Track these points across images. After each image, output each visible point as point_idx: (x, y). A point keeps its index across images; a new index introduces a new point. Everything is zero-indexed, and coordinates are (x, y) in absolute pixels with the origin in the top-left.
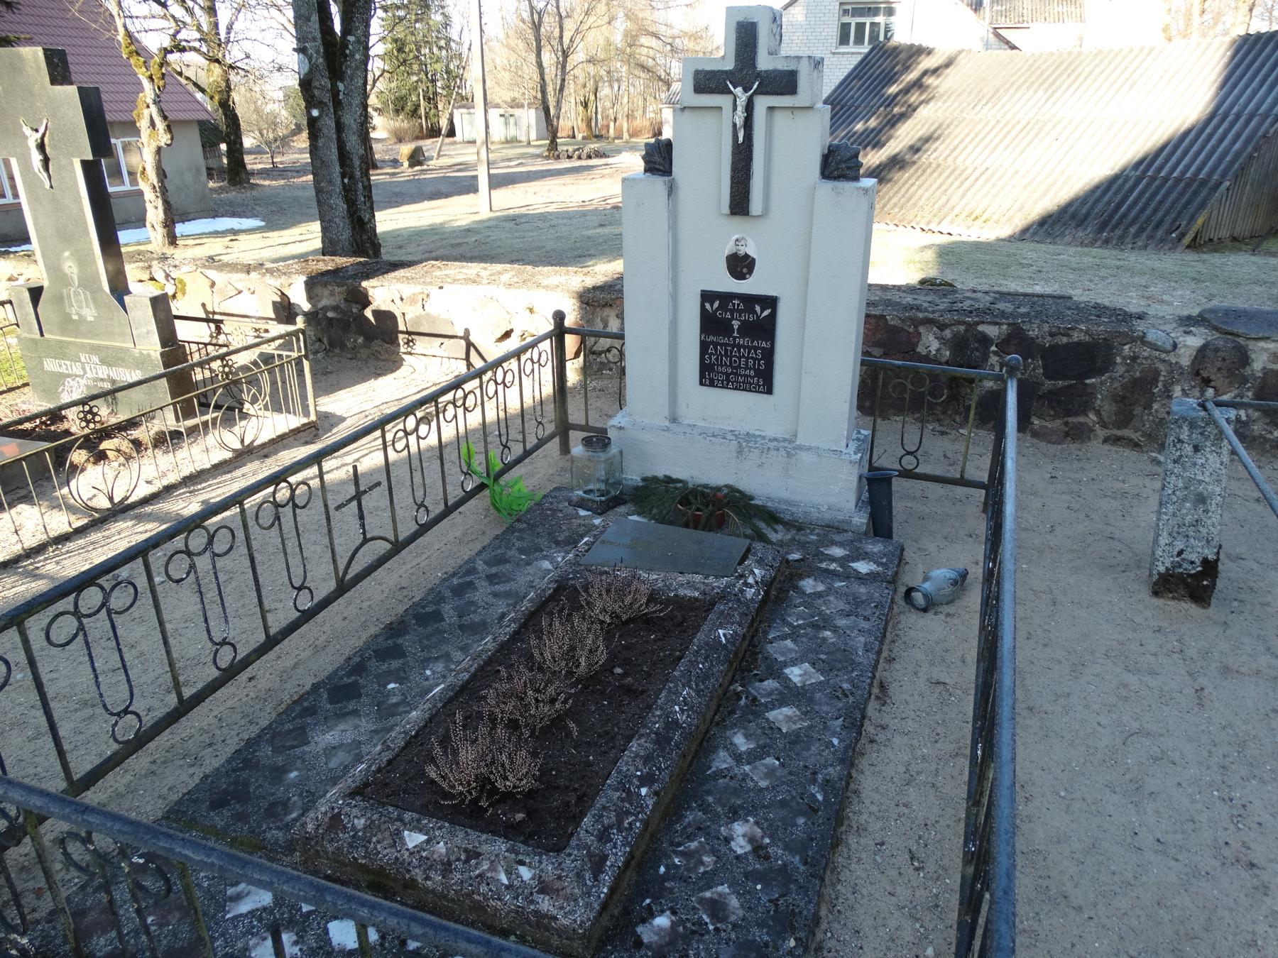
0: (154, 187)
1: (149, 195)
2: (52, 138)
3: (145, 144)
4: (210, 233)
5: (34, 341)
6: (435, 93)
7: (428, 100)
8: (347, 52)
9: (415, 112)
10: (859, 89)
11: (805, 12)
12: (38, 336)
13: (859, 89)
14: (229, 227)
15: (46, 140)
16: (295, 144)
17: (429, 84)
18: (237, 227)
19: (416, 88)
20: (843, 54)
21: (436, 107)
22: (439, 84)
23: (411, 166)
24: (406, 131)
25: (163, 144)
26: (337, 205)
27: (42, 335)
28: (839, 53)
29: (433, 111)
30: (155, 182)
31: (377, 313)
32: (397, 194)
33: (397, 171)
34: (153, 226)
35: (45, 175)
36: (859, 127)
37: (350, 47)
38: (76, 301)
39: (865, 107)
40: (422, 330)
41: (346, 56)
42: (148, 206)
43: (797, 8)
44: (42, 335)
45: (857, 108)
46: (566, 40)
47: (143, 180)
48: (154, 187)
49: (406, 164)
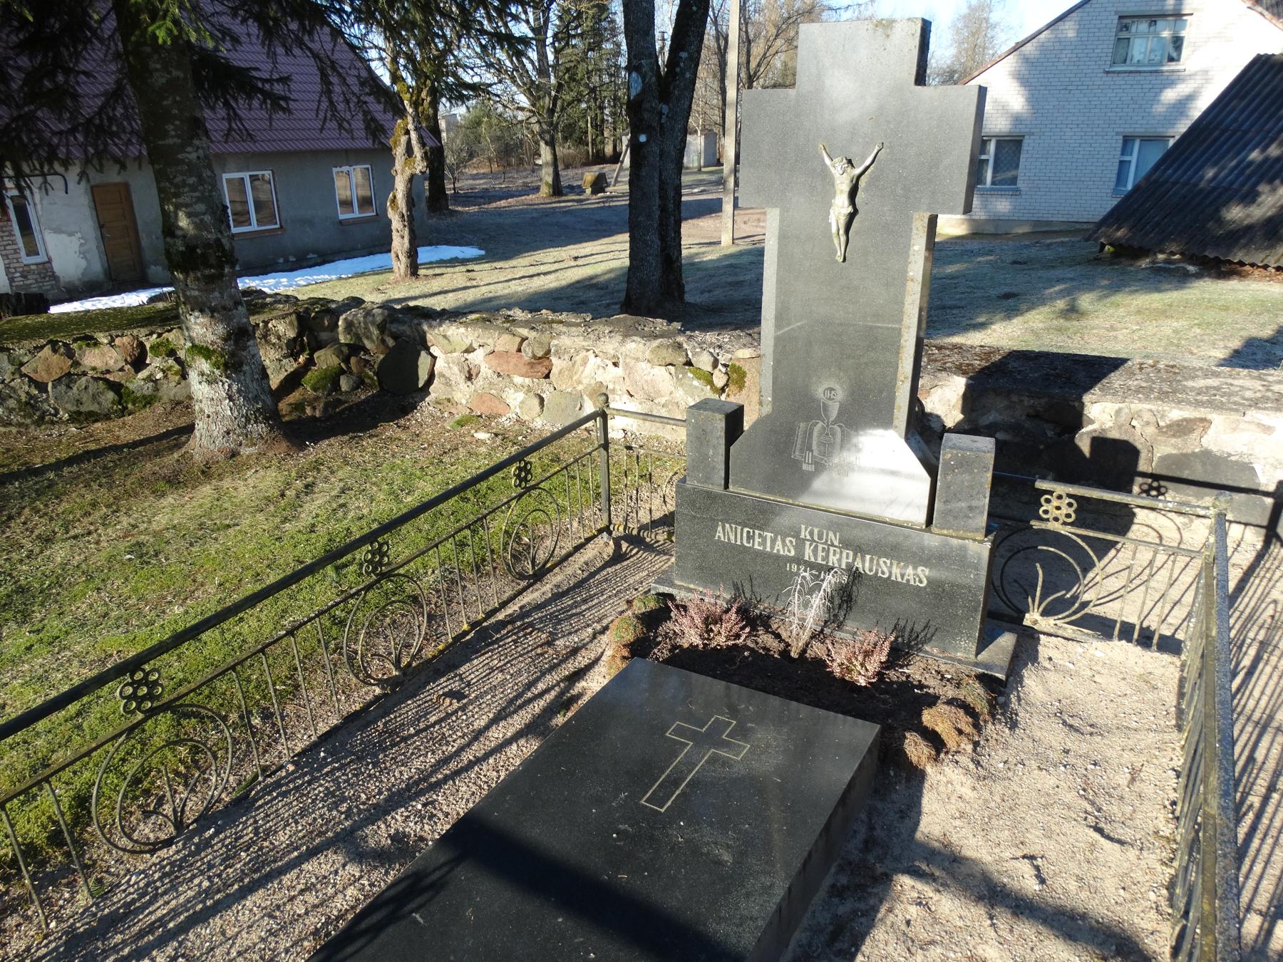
0: (403, 216)
1: (396, 224)
2: (869, 184)
3: (399, 172)
4: (437, 262)
5: (710, 496)
6: (603, 121)
7: (595, 126)
8: (678, 70)
9: (581, 141)
10: (1242, 111)
11: (1077, 27)
12: (719, 489)
13: (1242, 111)
14: (453, 256)
15: (863, 183)
16: (467, 170)
17: (598, 111)
18: (461, 256)
19: (585, 116)
20: (1119, 72)
21: (603, 134)
22: (607, 111)
23: (594, 192)
24: (574, 157)
25: (418, 172)
26: (652, 242)
27: (726, 487)
28: (1114, 72)
29: (599, 138)
30: (404, 212)
31: (1099, 442)
32: (601, 222)
33: (581, 197)
34: (397, 256)
35: (843, 239)
36: (1255, 155)
37: (682, 65)
38: (821, 444)
39: (1258, 133)
40: (1186, 474)
41: (676, 74)
42: (395, 235)
43: (1068, 23)
44: (726, 487)
45: (1245, 133)
46: (753, 65)
47: (392, 209)
48: (403, 216)
49: (589, 191)
